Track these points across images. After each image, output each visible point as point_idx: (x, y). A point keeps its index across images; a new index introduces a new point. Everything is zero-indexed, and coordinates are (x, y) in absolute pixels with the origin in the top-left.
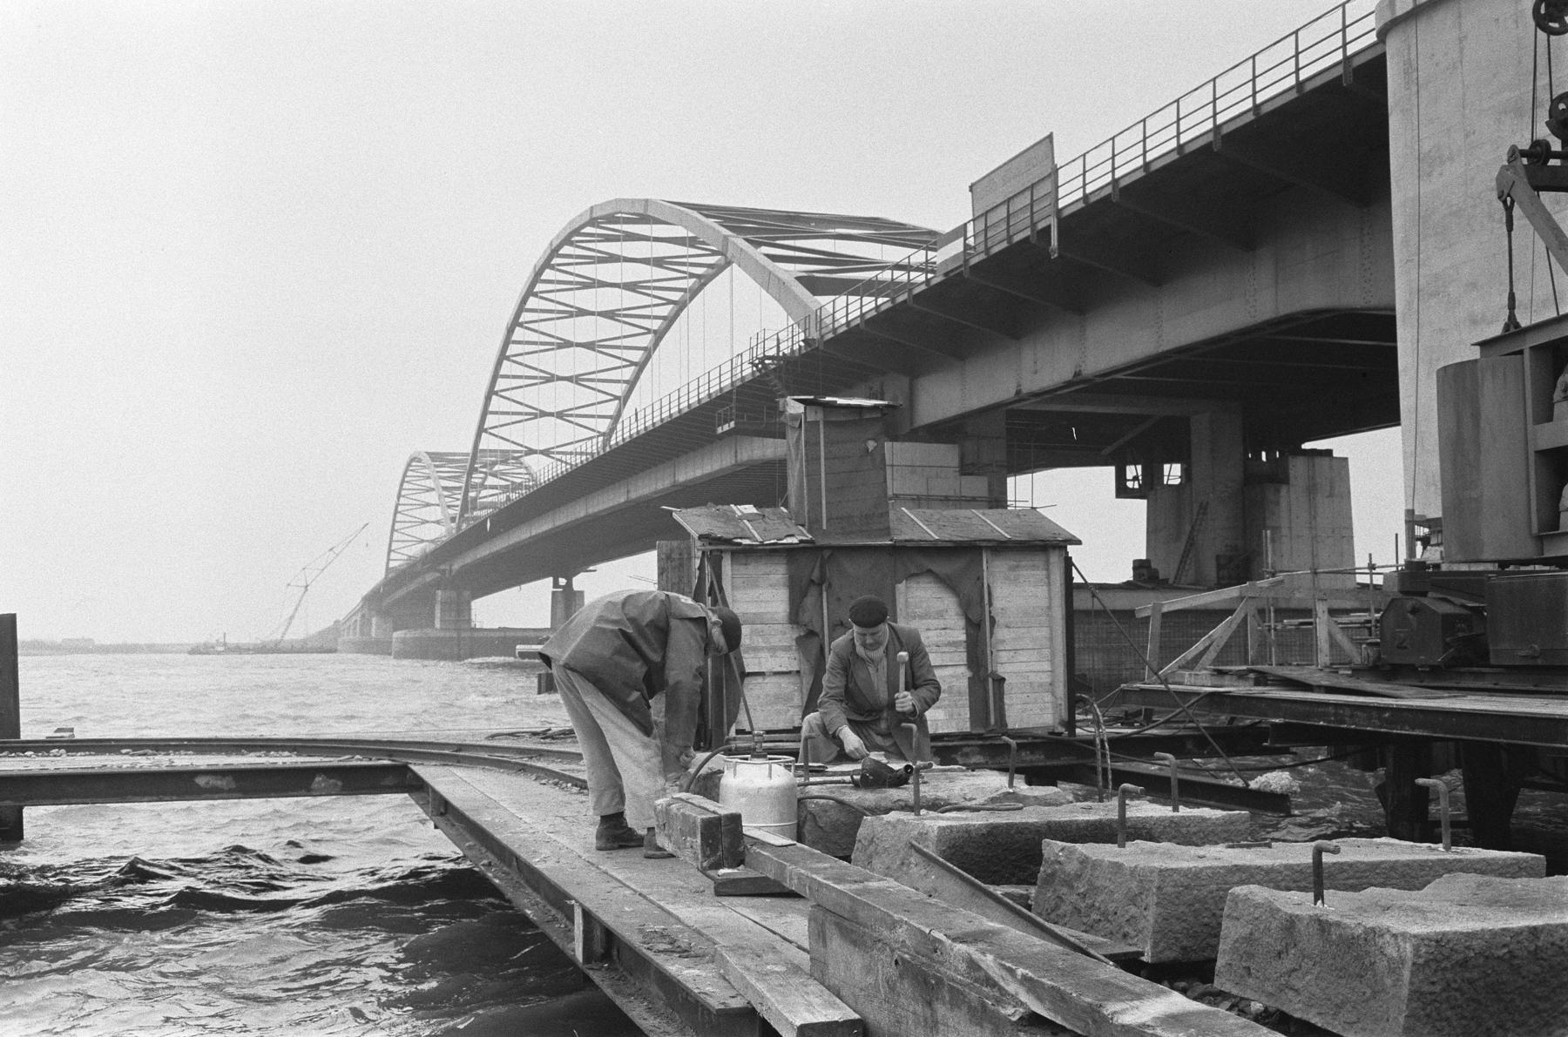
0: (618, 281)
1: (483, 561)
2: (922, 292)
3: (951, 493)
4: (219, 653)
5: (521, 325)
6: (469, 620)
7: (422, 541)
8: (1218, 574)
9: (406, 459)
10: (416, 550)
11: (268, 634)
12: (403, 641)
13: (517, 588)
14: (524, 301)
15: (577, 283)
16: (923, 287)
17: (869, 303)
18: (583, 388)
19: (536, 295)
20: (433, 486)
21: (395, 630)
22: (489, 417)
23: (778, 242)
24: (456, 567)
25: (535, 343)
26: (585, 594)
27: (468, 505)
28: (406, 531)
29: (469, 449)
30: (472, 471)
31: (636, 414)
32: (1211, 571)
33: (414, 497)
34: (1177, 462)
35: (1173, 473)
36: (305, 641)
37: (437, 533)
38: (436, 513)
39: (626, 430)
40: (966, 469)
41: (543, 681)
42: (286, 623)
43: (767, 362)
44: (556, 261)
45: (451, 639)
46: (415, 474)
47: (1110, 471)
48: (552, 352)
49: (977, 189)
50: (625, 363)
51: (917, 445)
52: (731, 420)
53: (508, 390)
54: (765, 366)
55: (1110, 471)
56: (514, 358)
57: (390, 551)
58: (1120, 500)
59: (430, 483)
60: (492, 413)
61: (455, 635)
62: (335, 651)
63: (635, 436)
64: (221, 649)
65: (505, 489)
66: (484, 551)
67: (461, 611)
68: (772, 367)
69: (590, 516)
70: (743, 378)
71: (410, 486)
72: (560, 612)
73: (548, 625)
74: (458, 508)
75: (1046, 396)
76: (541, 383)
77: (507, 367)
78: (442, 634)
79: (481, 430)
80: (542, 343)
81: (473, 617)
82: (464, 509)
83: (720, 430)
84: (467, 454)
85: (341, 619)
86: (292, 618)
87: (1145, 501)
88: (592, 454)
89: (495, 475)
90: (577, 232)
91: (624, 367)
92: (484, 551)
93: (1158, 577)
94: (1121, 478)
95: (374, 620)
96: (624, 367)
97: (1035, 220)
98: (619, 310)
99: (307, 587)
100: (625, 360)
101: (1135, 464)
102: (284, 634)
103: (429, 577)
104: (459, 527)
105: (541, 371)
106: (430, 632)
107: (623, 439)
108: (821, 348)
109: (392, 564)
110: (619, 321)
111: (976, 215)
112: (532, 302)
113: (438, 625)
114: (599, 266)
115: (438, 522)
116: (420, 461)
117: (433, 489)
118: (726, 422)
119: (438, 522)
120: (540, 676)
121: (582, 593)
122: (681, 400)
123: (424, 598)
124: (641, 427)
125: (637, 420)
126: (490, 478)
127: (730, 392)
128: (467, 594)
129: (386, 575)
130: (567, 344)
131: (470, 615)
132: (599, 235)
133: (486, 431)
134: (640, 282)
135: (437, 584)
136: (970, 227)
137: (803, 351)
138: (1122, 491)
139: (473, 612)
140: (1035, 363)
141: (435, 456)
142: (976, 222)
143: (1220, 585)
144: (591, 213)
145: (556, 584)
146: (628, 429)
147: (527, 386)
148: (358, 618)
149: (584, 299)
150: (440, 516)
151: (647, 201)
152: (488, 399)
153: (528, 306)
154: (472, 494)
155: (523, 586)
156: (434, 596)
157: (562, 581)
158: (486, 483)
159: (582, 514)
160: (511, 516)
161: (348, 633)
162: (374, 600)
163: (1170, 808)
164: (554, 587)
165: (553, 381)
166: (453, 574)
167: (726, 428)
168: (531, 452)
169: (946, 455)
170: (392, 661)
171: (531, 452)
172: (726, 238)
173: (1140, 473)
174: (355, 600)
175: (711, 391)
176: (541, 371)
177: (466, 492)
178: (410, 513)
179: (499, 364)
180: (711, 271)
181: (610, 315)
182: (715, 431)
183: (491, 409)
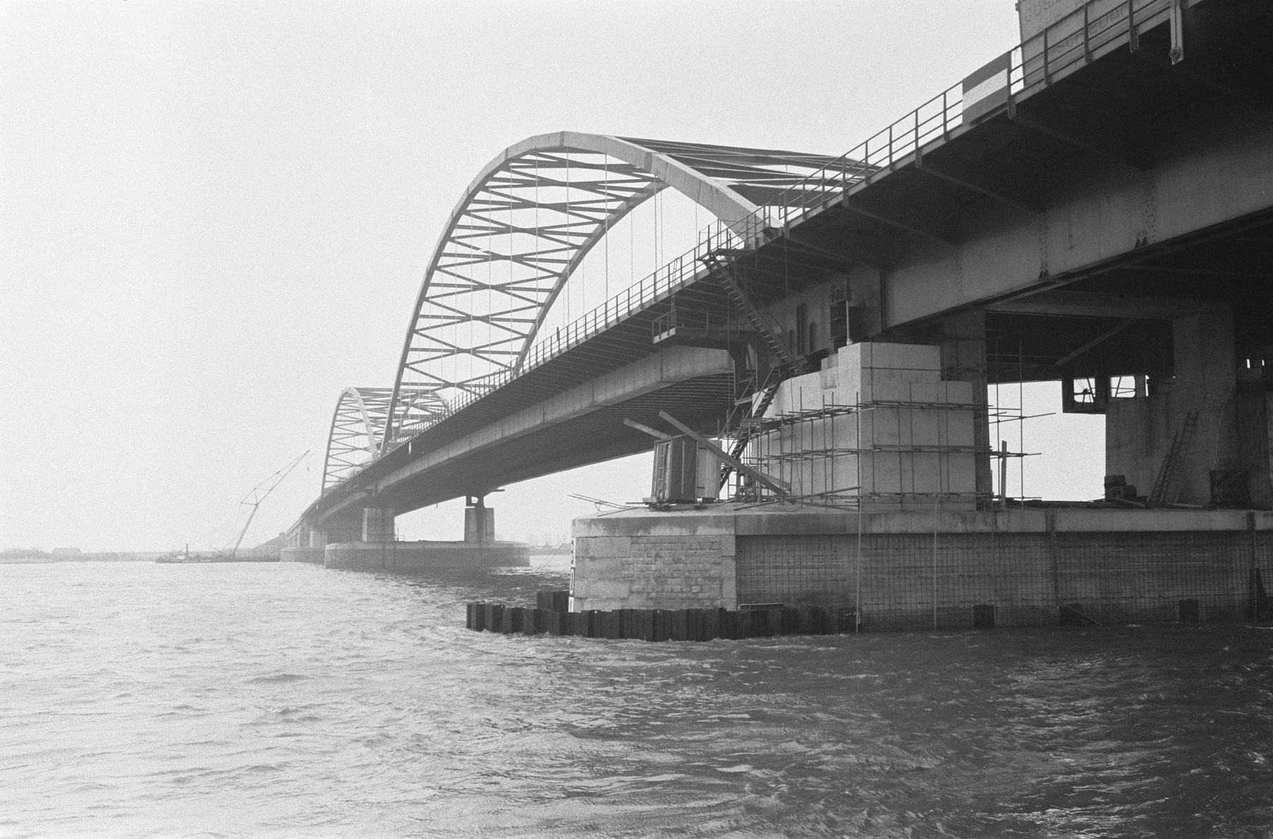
0: (474, 322)
1: (405, 483)
2: (862, 190)
3: (932, 400)
4: (181, 561)
5: (439, 269)
6: (393, 534)
7: (353, 465)
8: (1212, 490)
9: (339, 394)
10: (346, 473)
11: (223, 544)
12: (335, 552)
13: (434, 506)
14: (442, 245)
15: (493, 229)
16: (888, 172)
17: (795, 213)
19: (453, 240)
20: (361, 417)
21: (329, 543)
22: (411, 353)
24: (381, 487)
25: (453, 286)
26: (495, 512)
27: (390, 432)
28: (338, 457)
29: (392, 385)
30: (394, 403)
31: (558, 333)
32: (1203, 487)
33: (345, 427)
34: (1127, 373)
35: (1124, 386)
36: (254, 551)
37: (364, 458)
38: (364, 441)
39: (540, 354)
40: (949, 373)
41: (473, 614)
42: (239, 536)
43: (719, 258)
44: (472, 207)
45: (377, 550)
46: (346, 407)
47: (1057, 386)
48: (469, 293)
49: (1024, 7)
51: (896, 345)
52: (671, 328)
53: (427, 328)
54: (717, 263)
55: (1057, 386)
56: (446, 269)
57: (325, 473)
58: (1066, 414)
59: (359, 416)
60: (434, 285)
61: (380, 547)
62: (278, 560)
63: (556, 355)
64: (182, 558)
65: (424, 419)
66: (405, 473)
67: (385, 526)
68: (723, 264)
69: (474, 450)
70: (682, 282)
71: (343, 418)
72: (473, 527)
73: (462, 539)
74: (382, 437)
75: (1013, 298)
76: (458, 322)
77: (417, 341)
78: (368, 547)
79: (403, 365)
80: (459, 286)
81: (396, 532)
82: (388, 437)
83: (657, 339)
84: (390, 390)
85: (285, 532)
86: (244, 531)
87: (1103, 417)
88: (494, 386)
89: (415, 406)
90: (490, 177)
92: (405, 473)
93: (1135, 495)
94: (1068, 393)
95: (312, 534)
97: (1136, 21)
99: (257, 505)
101: (1087, 376)
102: (238, 544)
103: (358, 496)
104: (384, 452)
105: (459, 312)
106: (360, 546)
107: (544, 359)
108: (787, 236)
109: (327, 485)
110: (509, 294)
111: (1026, 39)
112: (450, 247)
113: (365, 537)
114: (515, 211)
115: (365, 449)
116: (351, 396)
117: (361, 421)
118: (665, 329)
119: (365, 449)
120: (469, 606)
121: (492, 510)
122: (588, 326)
123: (353, 515)
124: (563, 346)
125: (558, 339)
126: (412, 408)
127: (667, 300)
128: (391, 511)
129: (322, 495)
130: (481, 287)
131: (393, 529)
132: (515, 180)
133: (417, 332)
134: (526, 255)
135: (364, 503)
136: (1017, 59)
137: (762, 244)
138: (1070, 405)
139: (396, 527)
140: (1070, 236)
141: (363, 391)
142: (1027, 48)
143: (1214, 505)
144: (507, 155)
145: (469, 503)
146: (547, 346)
147: (444, 325)
148: (299, 530)
149: (481, 272)
150: (366, 444)
151: (563, 133)
152: (409, 337)
153: (446, 250)
154: (395, 425)
155: (440, 504)
156: (362, 513)
157: (475, 500)
158: (409, 413)
159: (498, 436)
160: (429, 441)
161: (291, 543)
162: (312, 516)
164: (468, 505)
165: (509, 232)
166: (379, 492)
167: (665, 336)
168: (448, 385)
169: (927, 357)
170: (322, 571)
171: (448, 385)
172: (648, 154)
173: (1093, 385)
174: (297, 517)
175: (644, 301)
176: (459, 312)
177: (390, 422)
178: (342, 441)
179: (419, 306)
180: (613, 216)
181: (519, 259)
182: (651, 340)
183: (412, 346)
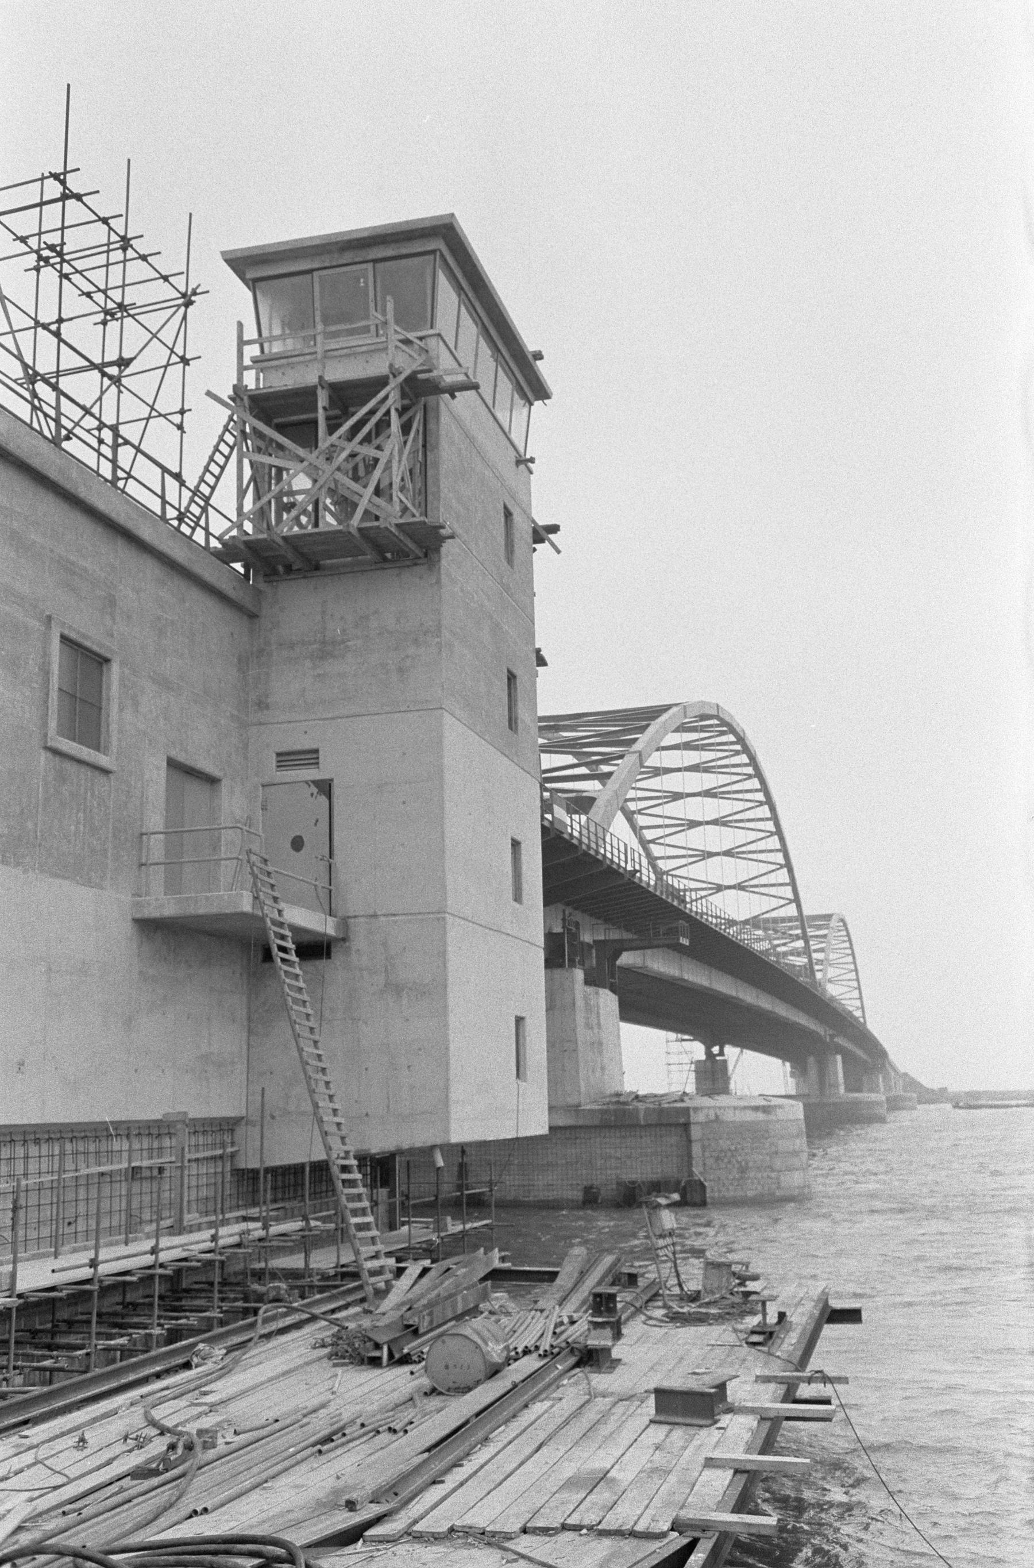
0: (689, 799)
18: (177, 327)
23: (585, 750)
48: (683, 833)
50: (661, 841)
91: (661, 837)
96: (661, 837)
98: (715, 788)
100: (662, 844)
110: (665, 792)
163: (324, 404)
